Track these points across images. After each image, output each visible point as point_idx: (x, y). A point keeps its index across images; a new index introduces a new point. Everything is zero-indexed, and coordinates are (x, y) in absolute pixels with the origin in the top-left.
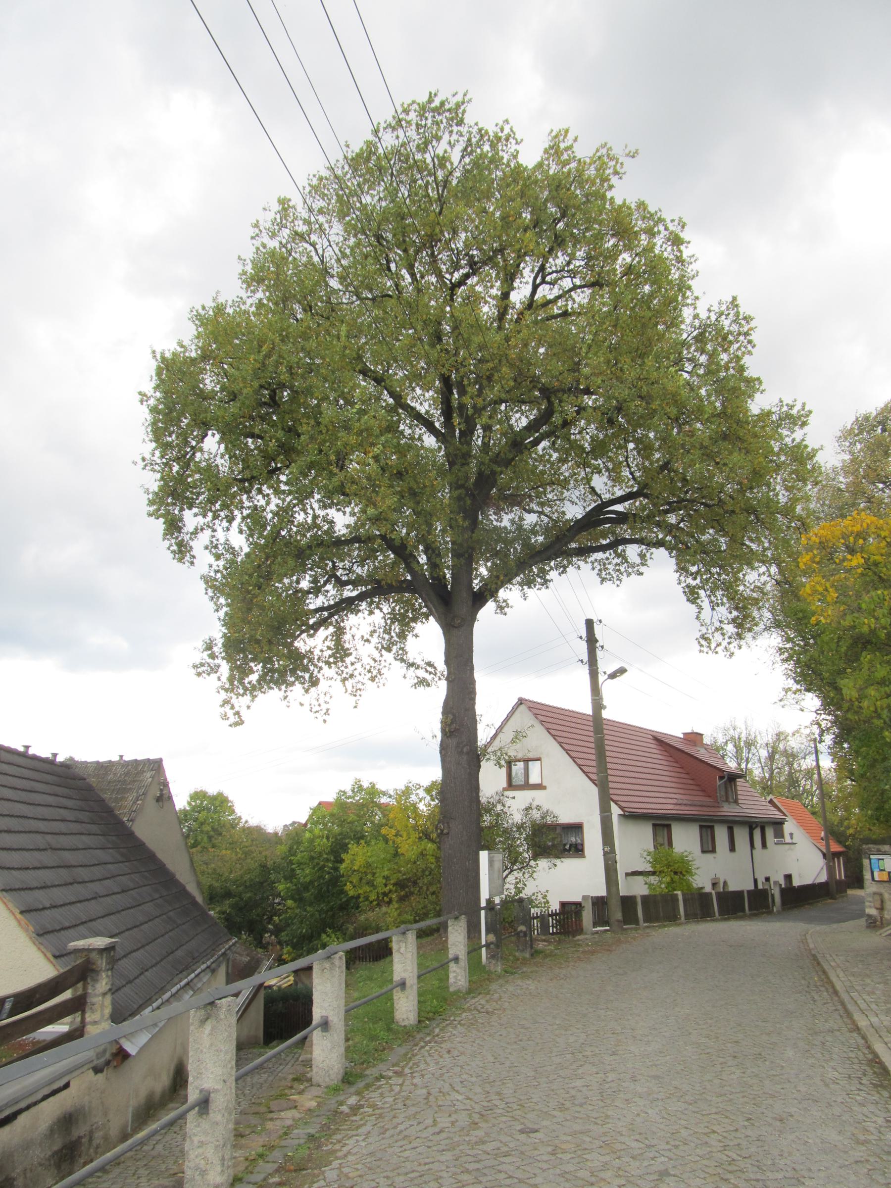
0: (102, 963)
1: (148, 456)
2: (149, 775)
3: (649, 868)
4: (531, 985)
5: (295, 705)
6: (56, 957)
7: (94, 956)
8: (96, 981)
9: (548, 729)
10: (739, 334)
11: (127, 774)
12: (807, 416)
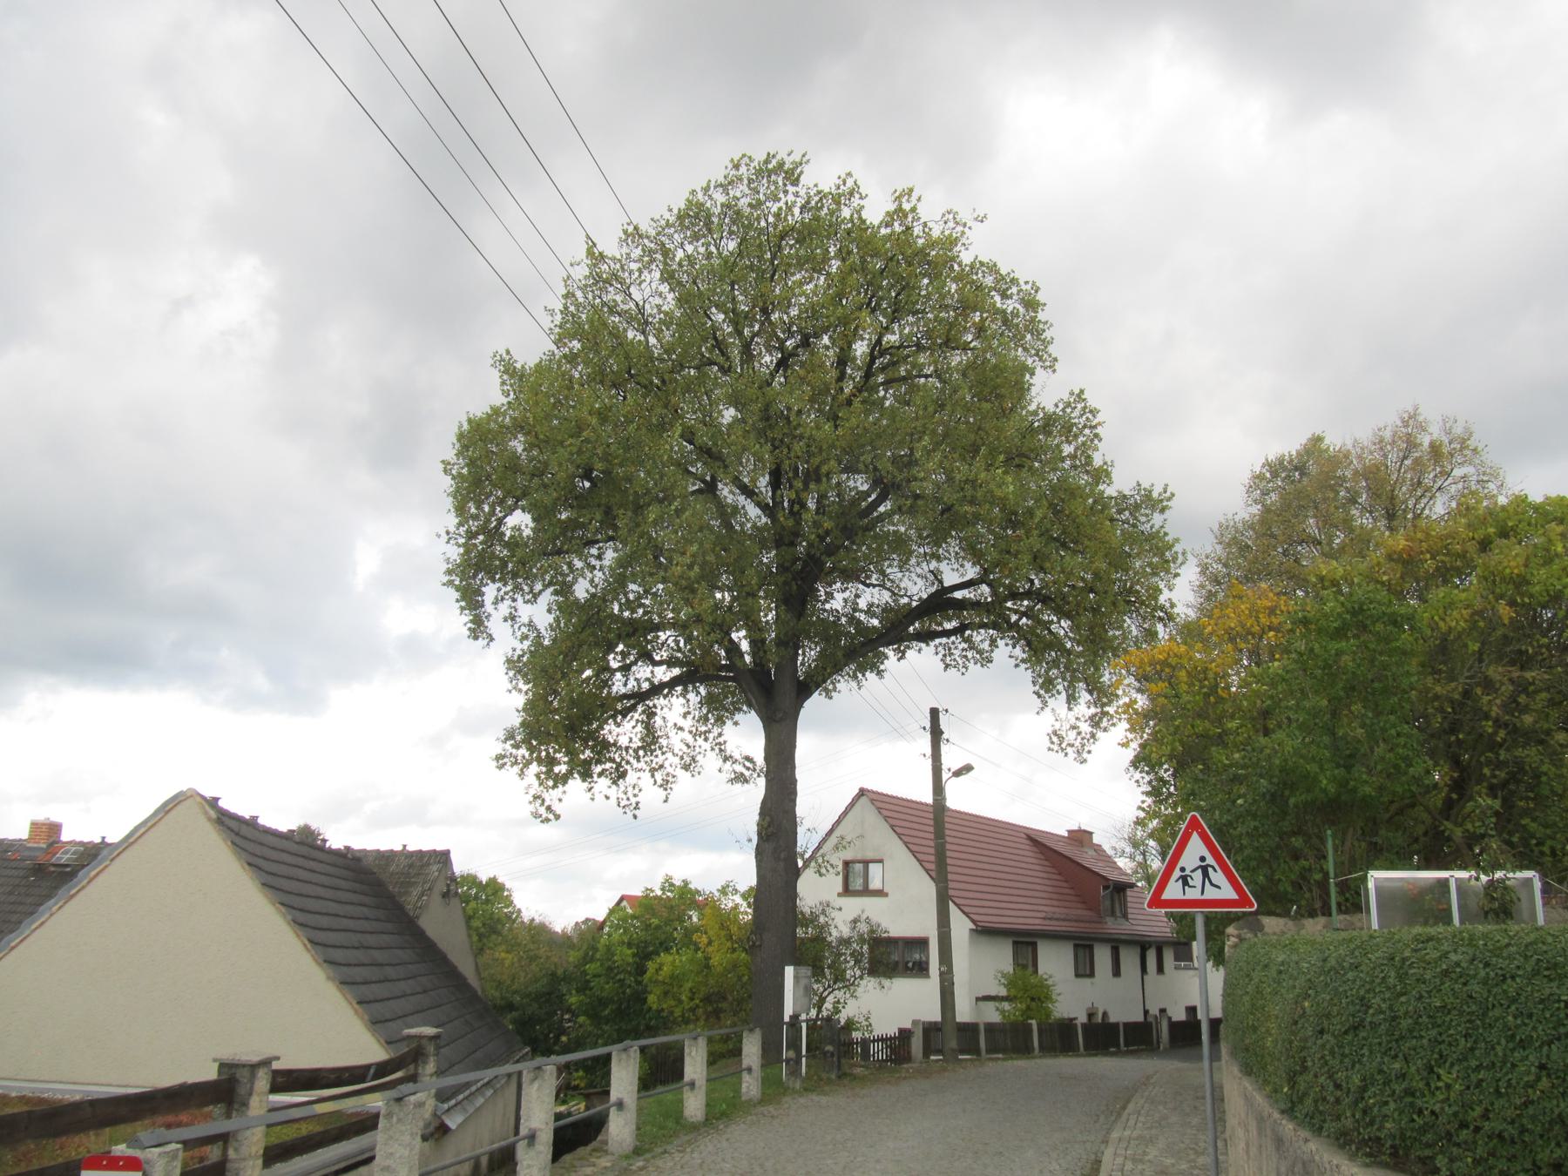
0: (431, 1049)
1: (452, 529)
2: (435, 868)
3: (1003, 992)
4: (824, 1100)
5: (599, 798)
6: (388, 1043)
7: (424, 1042)
8: (425, 1063)
9: (892, 827)
10: (1085, 426)
11: (411, 866)
12: (1169, 499)
